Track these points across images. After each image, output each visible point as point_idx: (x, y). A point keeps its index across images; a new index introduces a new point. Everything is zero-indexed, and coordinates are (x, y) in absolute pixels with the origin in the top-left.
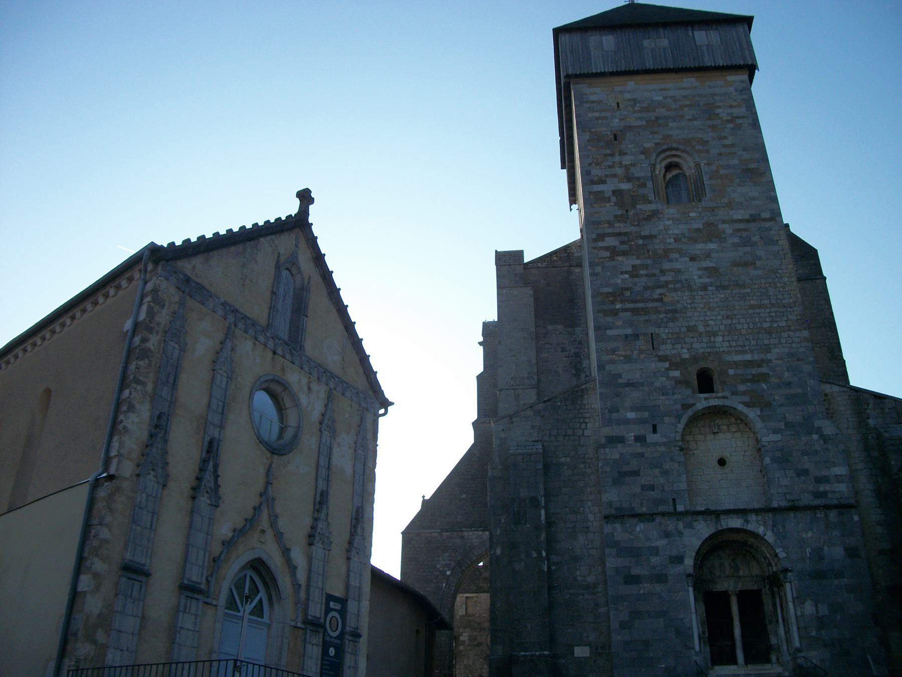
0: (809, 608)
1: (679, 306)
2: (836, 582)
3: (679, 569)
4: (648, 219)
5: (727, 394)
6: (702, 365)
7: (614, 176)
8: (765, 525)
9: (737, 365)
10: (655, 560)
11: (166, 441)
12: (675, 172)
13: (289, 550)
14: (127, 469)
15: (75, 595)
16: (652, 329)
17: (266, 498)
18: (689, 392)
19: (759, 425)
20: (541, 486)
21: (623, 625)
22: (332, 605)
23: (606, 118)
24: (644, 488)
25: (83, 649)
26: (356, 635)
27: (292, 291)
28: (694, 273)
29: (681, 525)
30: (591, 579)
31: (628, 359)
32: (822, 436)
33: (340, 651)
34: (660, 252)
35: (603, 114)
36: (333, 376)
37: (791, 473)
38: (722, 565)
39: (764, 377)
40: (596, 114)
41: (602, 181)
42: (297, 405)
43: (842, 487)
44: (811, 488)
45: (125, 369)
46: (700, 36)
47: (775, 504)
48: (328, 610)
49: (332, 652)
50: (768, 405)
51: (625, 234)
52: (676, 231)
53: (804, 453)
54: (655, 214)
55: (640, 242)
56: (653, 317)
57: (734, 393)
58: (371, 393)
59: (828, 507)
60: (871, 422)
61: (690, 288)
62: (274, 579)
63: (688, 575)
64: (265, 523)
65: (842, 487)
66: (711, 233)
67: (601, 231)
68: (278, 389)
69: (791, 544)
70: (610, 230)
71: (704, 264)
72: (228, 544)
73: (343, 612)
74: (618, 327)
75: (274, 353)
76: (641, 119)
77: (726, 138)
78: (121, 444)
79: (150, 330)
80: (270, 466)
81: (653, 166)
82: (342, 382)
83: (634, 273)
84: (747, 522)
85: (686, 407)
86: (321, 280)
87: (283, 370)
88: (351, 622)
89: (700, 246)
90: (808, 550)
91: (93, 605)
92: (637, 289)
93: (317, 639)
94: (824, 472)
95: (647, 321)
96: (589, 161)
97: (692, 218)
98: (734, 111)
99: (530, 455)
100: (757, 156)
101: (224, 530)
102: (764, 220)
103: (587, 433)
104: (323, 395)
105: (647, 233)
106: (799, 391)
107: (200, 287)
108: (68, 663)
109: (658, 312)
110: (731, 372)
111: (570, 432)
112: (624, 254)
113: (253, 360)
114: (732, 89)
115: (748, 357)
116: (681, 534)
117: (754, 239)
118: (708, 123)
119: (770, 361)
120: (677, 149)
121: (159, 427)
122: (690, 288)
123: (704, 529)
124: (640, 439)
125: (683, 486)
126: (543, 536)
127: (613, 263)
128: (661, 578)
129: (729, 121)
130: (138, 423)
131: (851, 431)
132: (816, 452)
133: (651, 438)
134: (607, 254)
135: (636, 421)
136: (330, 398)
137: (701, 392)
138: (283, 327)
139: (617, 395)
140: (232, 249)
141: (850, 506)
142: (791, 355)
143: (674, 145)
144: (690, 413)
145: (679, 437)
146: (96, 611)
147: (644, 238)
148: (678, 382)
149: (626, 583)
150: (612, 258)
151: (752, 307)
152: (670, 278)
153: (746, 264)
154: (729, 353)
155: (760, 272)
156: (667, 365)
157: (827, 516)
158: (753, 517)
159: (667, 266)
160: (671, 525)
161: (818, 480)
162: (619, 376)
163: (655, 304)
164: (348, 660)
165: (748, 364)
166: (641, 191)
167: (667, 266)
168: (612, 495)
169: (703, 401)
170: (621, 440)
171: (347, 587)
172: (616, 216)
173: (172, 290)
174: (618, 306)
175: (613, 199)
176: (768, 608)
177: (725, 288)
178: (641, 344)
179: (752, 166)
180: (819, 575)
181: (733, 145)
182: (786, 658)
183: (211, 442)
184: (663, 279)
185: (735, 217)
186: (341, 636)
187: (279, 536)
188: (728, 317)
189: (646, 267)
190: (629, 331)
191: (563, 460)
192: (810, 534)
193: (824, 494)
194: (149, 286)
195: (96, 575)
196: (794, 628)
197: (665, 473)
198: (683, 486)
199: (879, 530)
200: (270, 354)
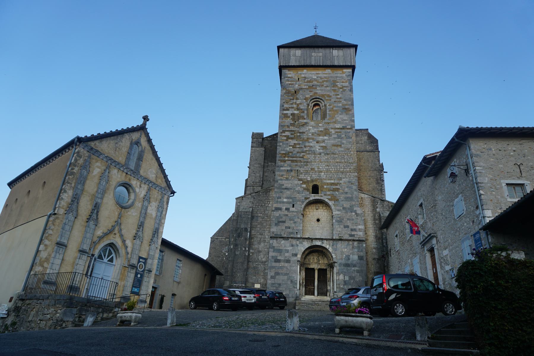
0: (341, 277)
1: (309, 160)
2: (353, 268)
3: (295, 258)
4: (303, 125)
5: (322, 195)
6: (315, 183)
7: (293, 108)
8: (329, 245)
9: (328, 184)
10: (287, 254)
11: (78, 203)
12: (317, 107)
13: (125, 241)
14: (62, 211)
15: (38, 251)
16: (298, 168)
17: (118, 223)
18: (308, 193)
19: (333, 207)
20: (249, 224)
21: (272, 277)
22: (141, 260)
23: (293, 84)
24: (286, 227)
25: (38, 269)
26: (150, 271)
27: (137, 152)
28: (317, 148)
29: (298, 242)
30: (264, 260)
31: (287, 179)
32: (356, 213)
33: (142, 276)
34: (305, 139)
35: (292, 83)
36: (151, 182)
37: (342, 226)
38: (314, 258)
39: (338, 190)
40: (290, 83)
41: (287, 110)
42: (134, 191)
43: (361, 233)
44: (349, 233)
45: (65, 178)
46: (335, 52)
47: (334, 238)
48: (139, 262)
49: (139, 276)
50: (337, 200)
51: (293, 131)
52: (313, 131)
53: (348, 219)
54: (306, 124)
55: (299, 134)
56: (299, 164)
57: (325, 195)
58: (167, 188)
59: (354, 240)
60: (378, 210)
61: (315, 153)
62: (118, 250)
63: (298, 261)
64: (116, 231)
65: (361, 233)
66: (326, 132)
67: (284, 129)
68: (128, 186)
69: (339, 253)
70: (288, 129)
71: (322, 145)
72: (101, 238)
73: (145, 263)
74: (285, 167)
75: (127, 174)
76: (307, 85)
77: (338, 95)
78: (60, 203)
79: (75, 166)
80: (121, 212)
81: (308, 105)
82: (155, 184)
83: (294, 146)
84: (323, 243)
85: (306, 198)
86: (150, 148)
87: (130, 180)
88: (148, 267)
89: (321, 137)
90: (344, 256)
91: (43, 255)
92: (295, 152)
93: (134, 271)
94: (355, 227)
95: (296, 165)
96: (284, 101)
97: (320, 126)
98: (344, 84)
99: (247, 212)
100: (349, 103)
101: (99, 233)
102: (348, 129)
103: (269, 205)
104: (146, 188)
105: (302, 131)
106: (350, 196)
107: (97, 151)
108: (32, 273)
109: (301, 162)
110: (325, 187)
111: (263, 205)
112: (292, 138)
113: (117, 176)
114: (344, 75)
115: (333, 181)
116: (298, 245)
117: (342, 136)
118: (333, 88)
119: (341, 183)
120: (319, 98)
121: (76, 199)
122: (315, 153)
123: (307, 245)
124: (287, 209)
125: (301, 228)
126: (248, 242)
127: (287, 142)
128: (288, 261)
129: (341, 88)
130: (67, 197)
131: (369, 212)
132: (353, 220)
133: (292, 209)
134: (285, 138)
135: (287, 203)
136: (149, 190)
137: (312, 193)
138: (132, 166)
139: (281, 192)
140: (112, 138)
141: (363, 241)
142: (349, 182)
143: (318, 97)
144: (307, 201)
145: (302, 210)
146: (45, 257)
147: (300, 133)
148: (304, 189)
149: (275, 262)
150: (287, 140)
151: (337, 162)
152: (307, 149)
153: (337, 146)
154: (325, 179)
155: (343, 149)
156: (301, 182)
157: (353, 244)
158: (325, 242)
159: (307, 144)
160: (294, 242)
161: (352, 230)
162: (283, 185)
163: (300, 159)
164: (145, 279)
165: (332, 184)
166: (302, 114)
167: (307, 144)
168: (274, 229)
169: (313, 197)
170: (280, 209)
171: (148, 254)
172: (291, 124)
173: (85, 152)
174: (286, 159)
175: (291, 117)
176: (328, 276)
177: (328, 154)
178: (293, 173)
179: (346, 107)
180: (347, 265)
181: (340, 98)
182: (332, 294)
183: (96, 204)
184: (305, 149)
185: (337, 127)
186: (143, 271)
187: (121, 236)
188: (327, 166)
189: (299, 144)
190: (289, 169)
191: (259, 215)
192: (346, 250)
193: (353, 235)
194: (77, 150)
195: (46, 245)
196: (335, 284)
197: (295, 223)
198: (301, 228)
199: (374, 250)
200: (124, 174)
